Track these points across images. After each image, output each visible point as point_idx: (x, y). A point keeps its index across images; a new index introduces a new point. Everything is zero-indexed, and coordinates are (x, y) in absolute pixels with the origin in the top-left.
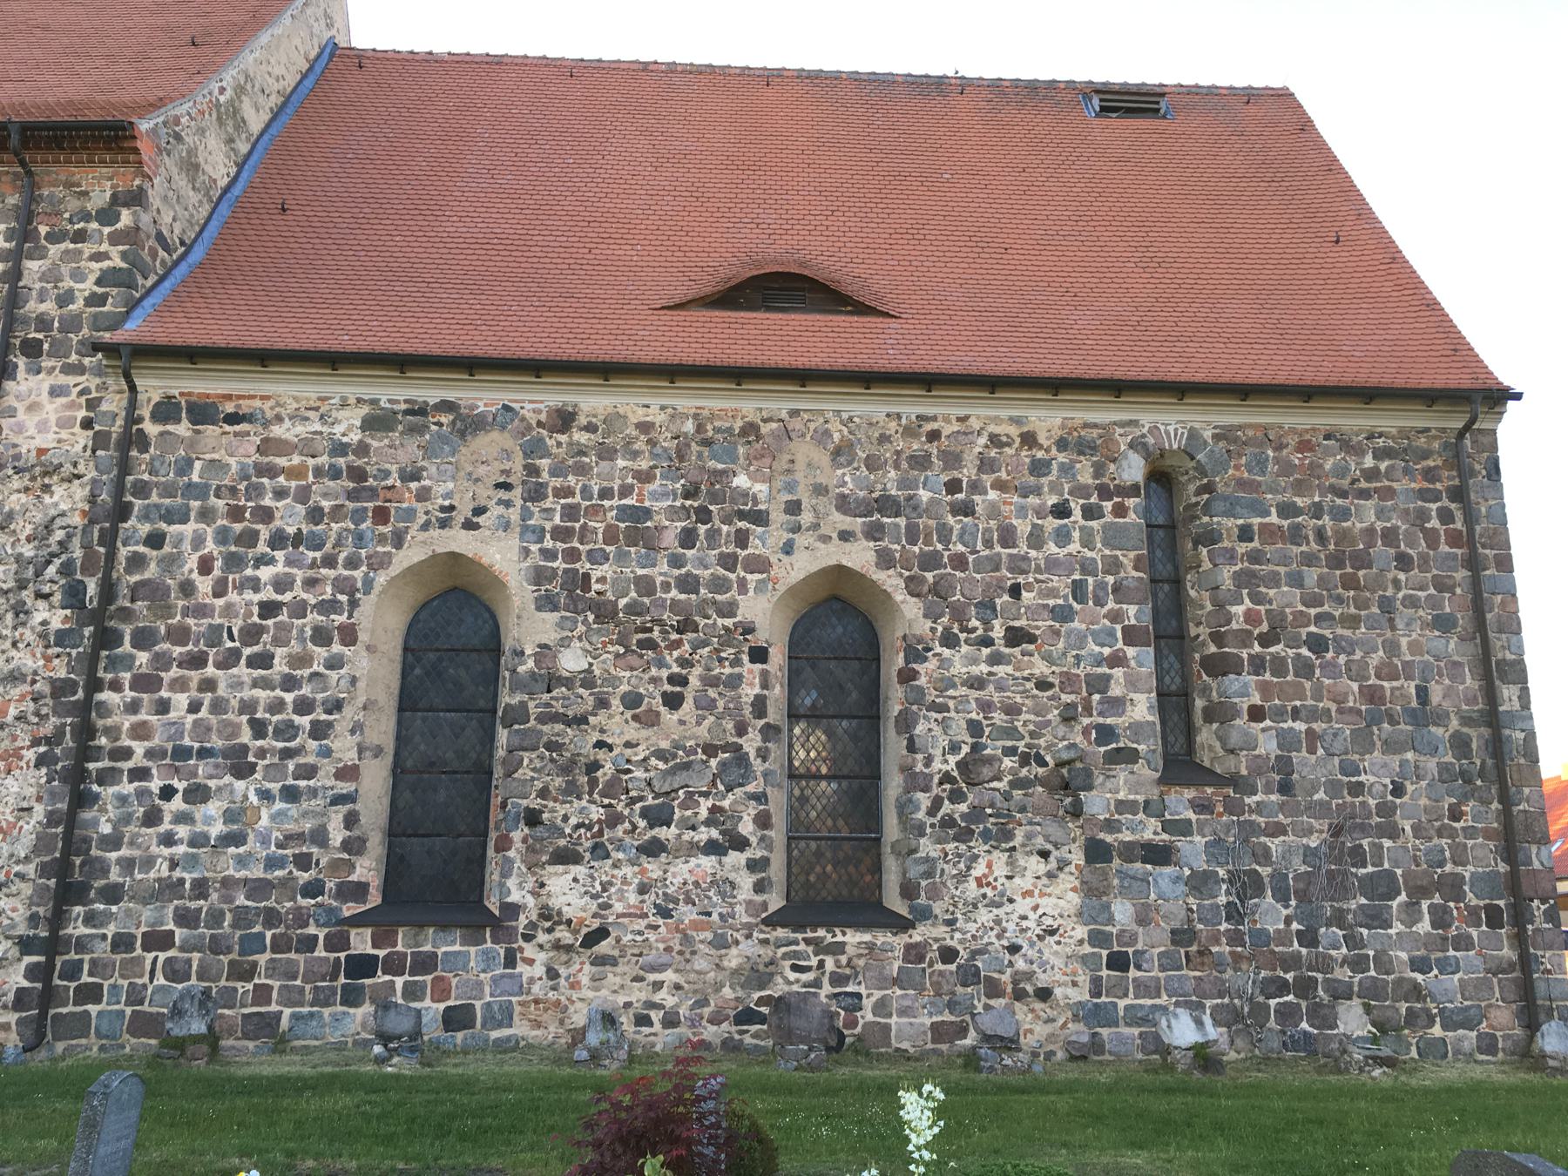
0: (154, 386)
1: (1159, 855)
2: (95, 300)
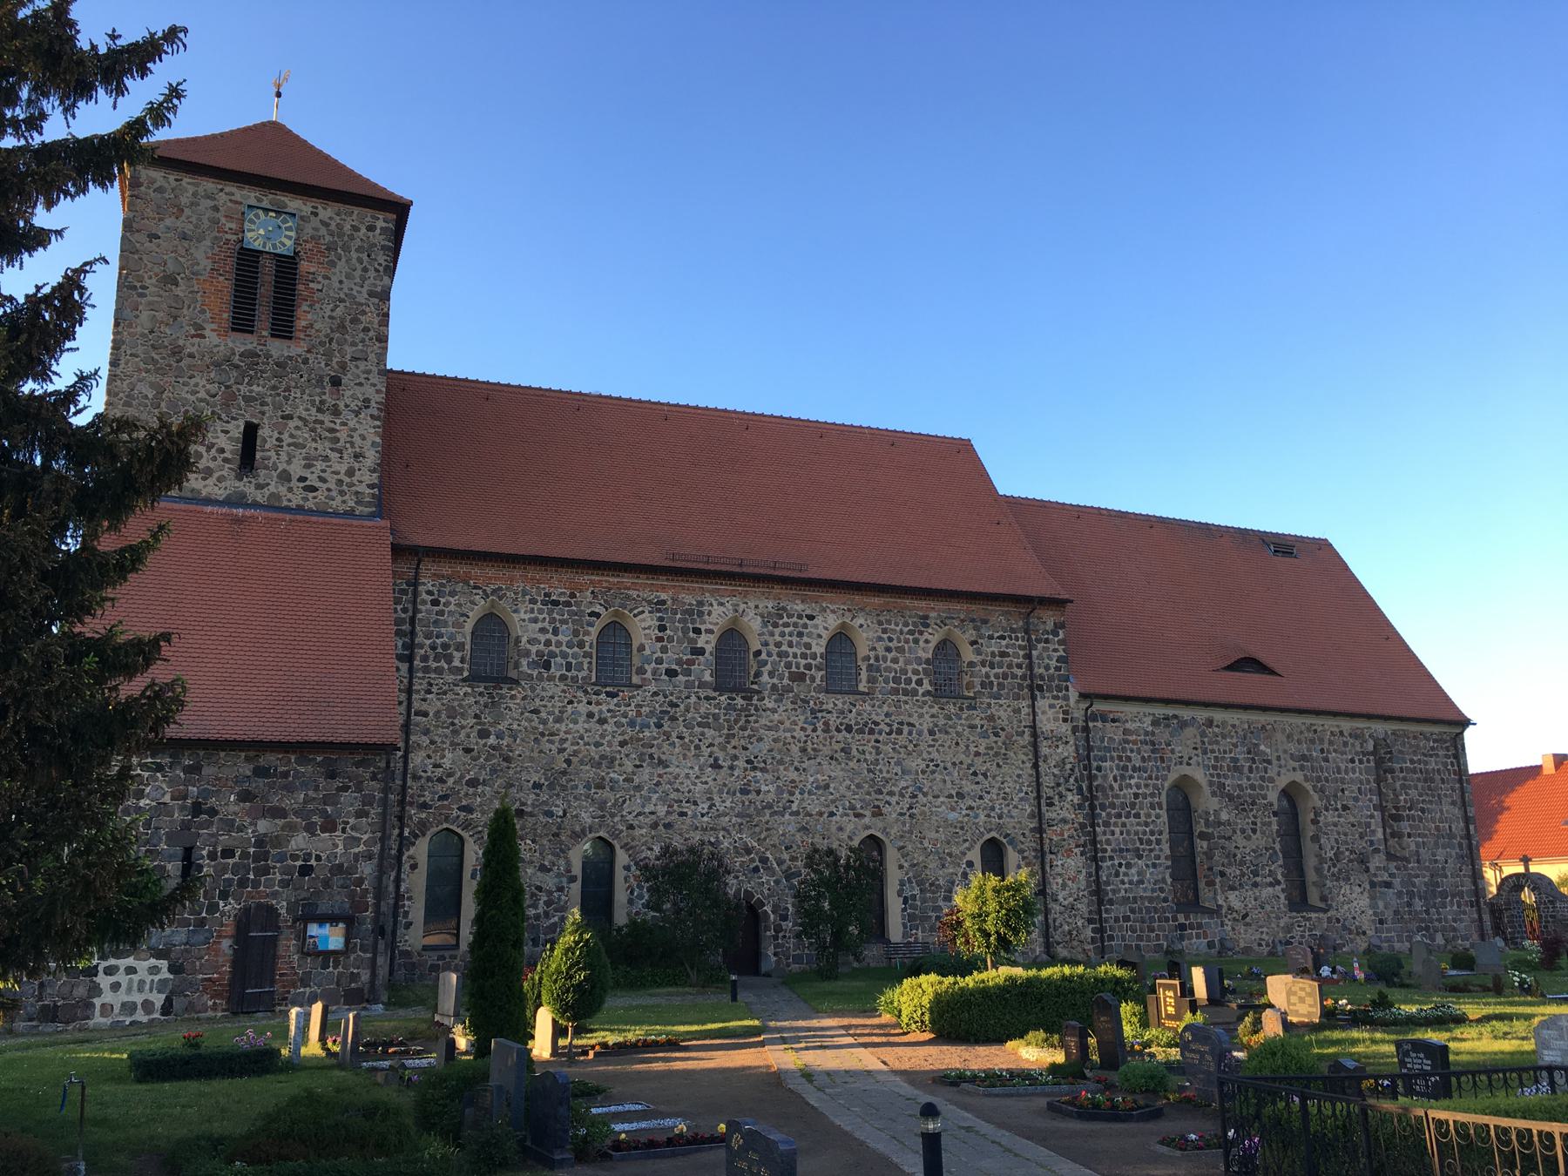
0: (1099, 706)
1: (1388, 885)
2: (1058, 669)
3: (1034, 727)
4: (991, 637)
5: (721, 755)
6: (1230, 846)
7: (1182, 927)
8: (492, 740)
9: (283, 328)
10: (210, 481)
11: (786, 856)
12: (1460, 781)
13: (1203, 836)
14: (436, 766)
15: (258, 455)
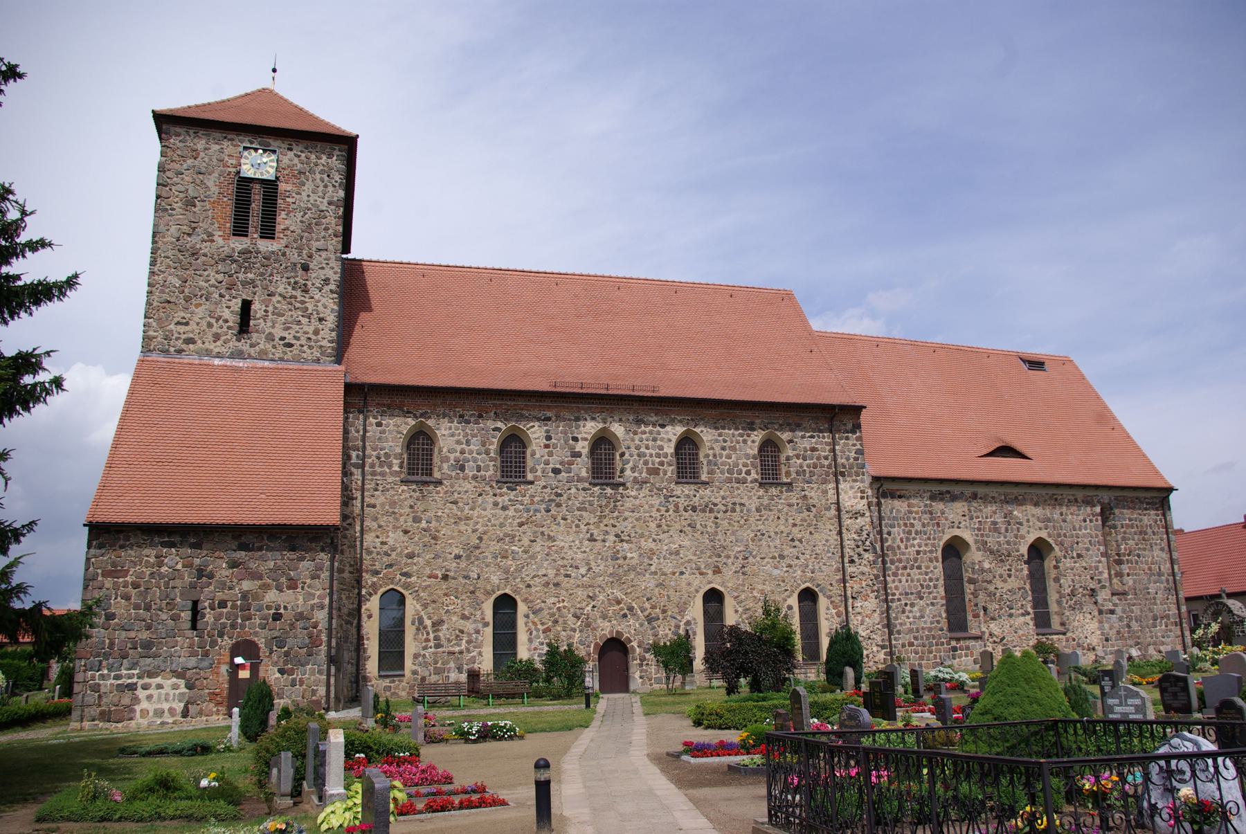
1: (1112, 612)
2: (856, 459)
3: (838, 503)
4: (803, 437)
5: (595, 532)
6: (991, 588)
7: (954, 649)
8: (424, 524)
9: (268, 232)
10: (218, 343)
11: (647, 605)
12: (1167, 533)
13: (971, 581)
14: (383, 543)
15: (252, 323)
